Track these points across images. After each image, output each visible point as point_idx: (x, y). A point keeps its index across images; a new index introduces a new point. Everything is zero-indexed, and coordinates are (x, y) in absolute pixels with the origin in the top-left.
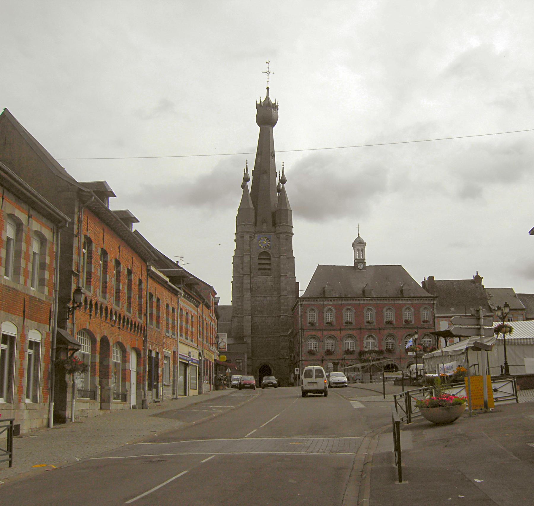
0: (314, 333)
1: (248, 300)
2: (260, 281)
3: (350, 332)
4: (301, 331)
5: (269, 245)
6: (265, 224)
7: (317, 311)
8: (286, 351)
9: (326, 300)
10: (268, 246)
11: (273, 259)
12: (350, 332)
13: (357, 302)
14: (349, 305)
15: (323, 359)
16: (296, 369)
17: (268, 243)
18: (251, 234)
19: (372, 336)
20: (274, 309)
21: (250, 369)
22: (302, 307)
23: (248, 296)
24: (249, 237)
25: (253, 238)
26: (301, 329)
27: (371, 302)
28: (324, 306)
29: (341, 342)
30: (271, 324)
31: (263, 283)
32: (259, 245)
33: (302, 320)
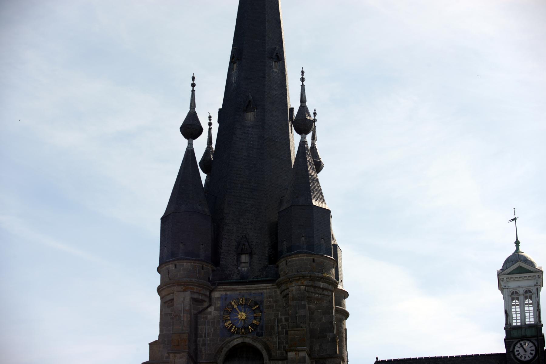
5: (255, 322)
6: (244, 258)
17: (255, 318)
25: (206, 304)
32: (226, 324)
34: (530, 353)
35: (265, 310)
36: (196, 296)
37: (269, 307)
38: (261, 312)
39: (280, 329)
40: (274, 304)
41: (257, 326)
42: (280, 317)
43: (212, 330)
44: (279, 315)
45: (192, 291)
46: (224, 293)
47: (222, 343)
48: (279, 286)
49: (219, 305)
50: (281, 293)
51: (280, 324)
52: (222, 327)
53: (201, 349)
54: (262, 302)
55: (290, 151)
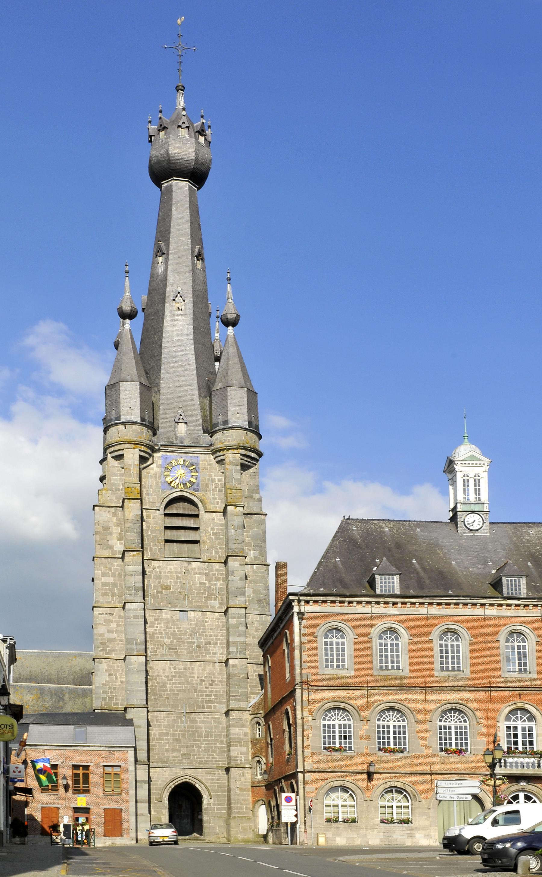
0: (342, 695)
1: (135, 617)
2: (171, 572)
3: (454, 697)
4: (302, 689)
7: (350, 634)
8: (244, 750)
9: (378, 603)
10: (190, 482)
11: (204, 517)
12: (454, 697)
13: (478, 611)
14: (452, 618)
15: (372, 769)
16: (284, 795)
17: (192, 476)
18: (143, 448)
19: (524, 710)
20: (210, 643)
21: (6, 774)
22: (304, 622)
23: (134, 606)
24: (137, 457)
26: (302, 682)
27: (522, 612)
28: (373, 619)
29: (429, 724)
30: (202, 681)
31: (178, 578)
33: (305, 657)
34: (164, 541)
35: (201, 470)
36: (143, 454)
37: (205, 468)
38: (197, 472)
39: (214, 487)
40: (209, 467)
41: (194, 483)
42: (213, 477)
43: (155, 483)
44: (213, 475)
45: (141, 449)
46: (164, 453)
47: (164, 495)
48: (214, 452)
49: (160, 463)
50: (215, 459)
51: (213, 483)
52: (163, 481)
53: (145, 497)
54: (197, 464)
55: (194, 333)
